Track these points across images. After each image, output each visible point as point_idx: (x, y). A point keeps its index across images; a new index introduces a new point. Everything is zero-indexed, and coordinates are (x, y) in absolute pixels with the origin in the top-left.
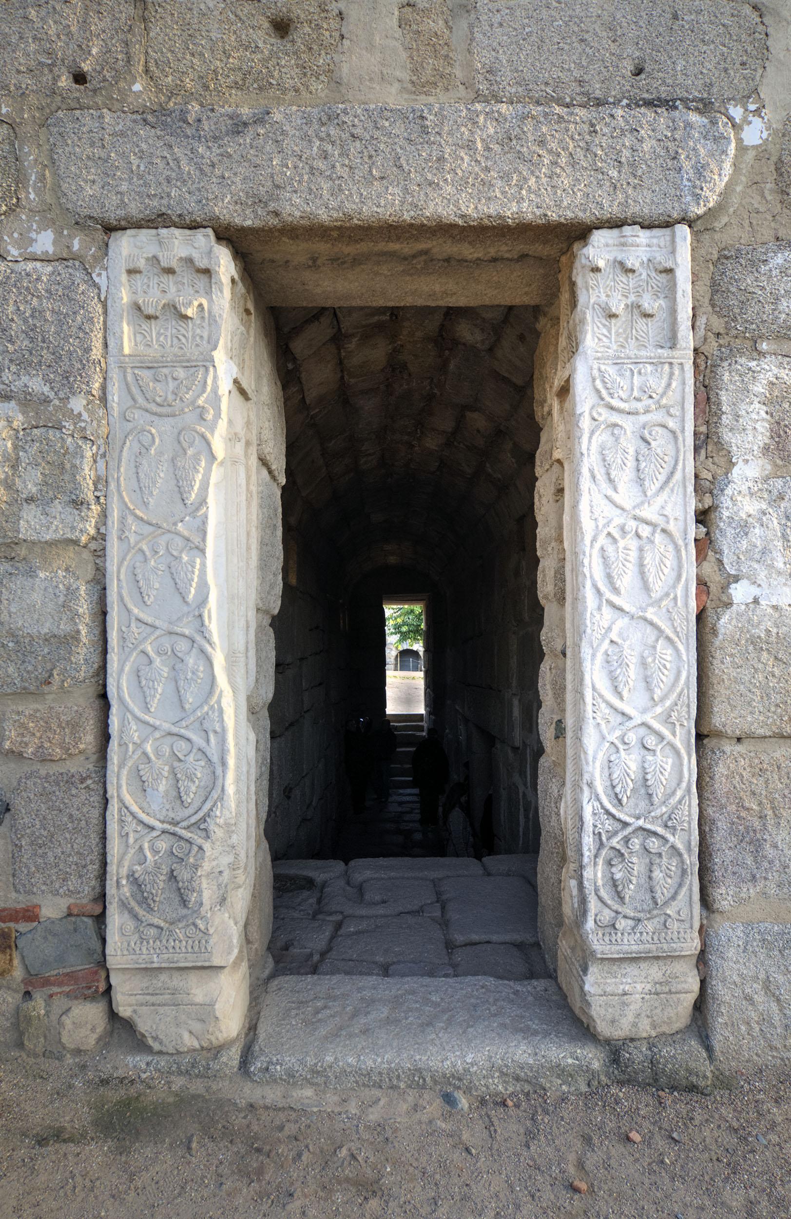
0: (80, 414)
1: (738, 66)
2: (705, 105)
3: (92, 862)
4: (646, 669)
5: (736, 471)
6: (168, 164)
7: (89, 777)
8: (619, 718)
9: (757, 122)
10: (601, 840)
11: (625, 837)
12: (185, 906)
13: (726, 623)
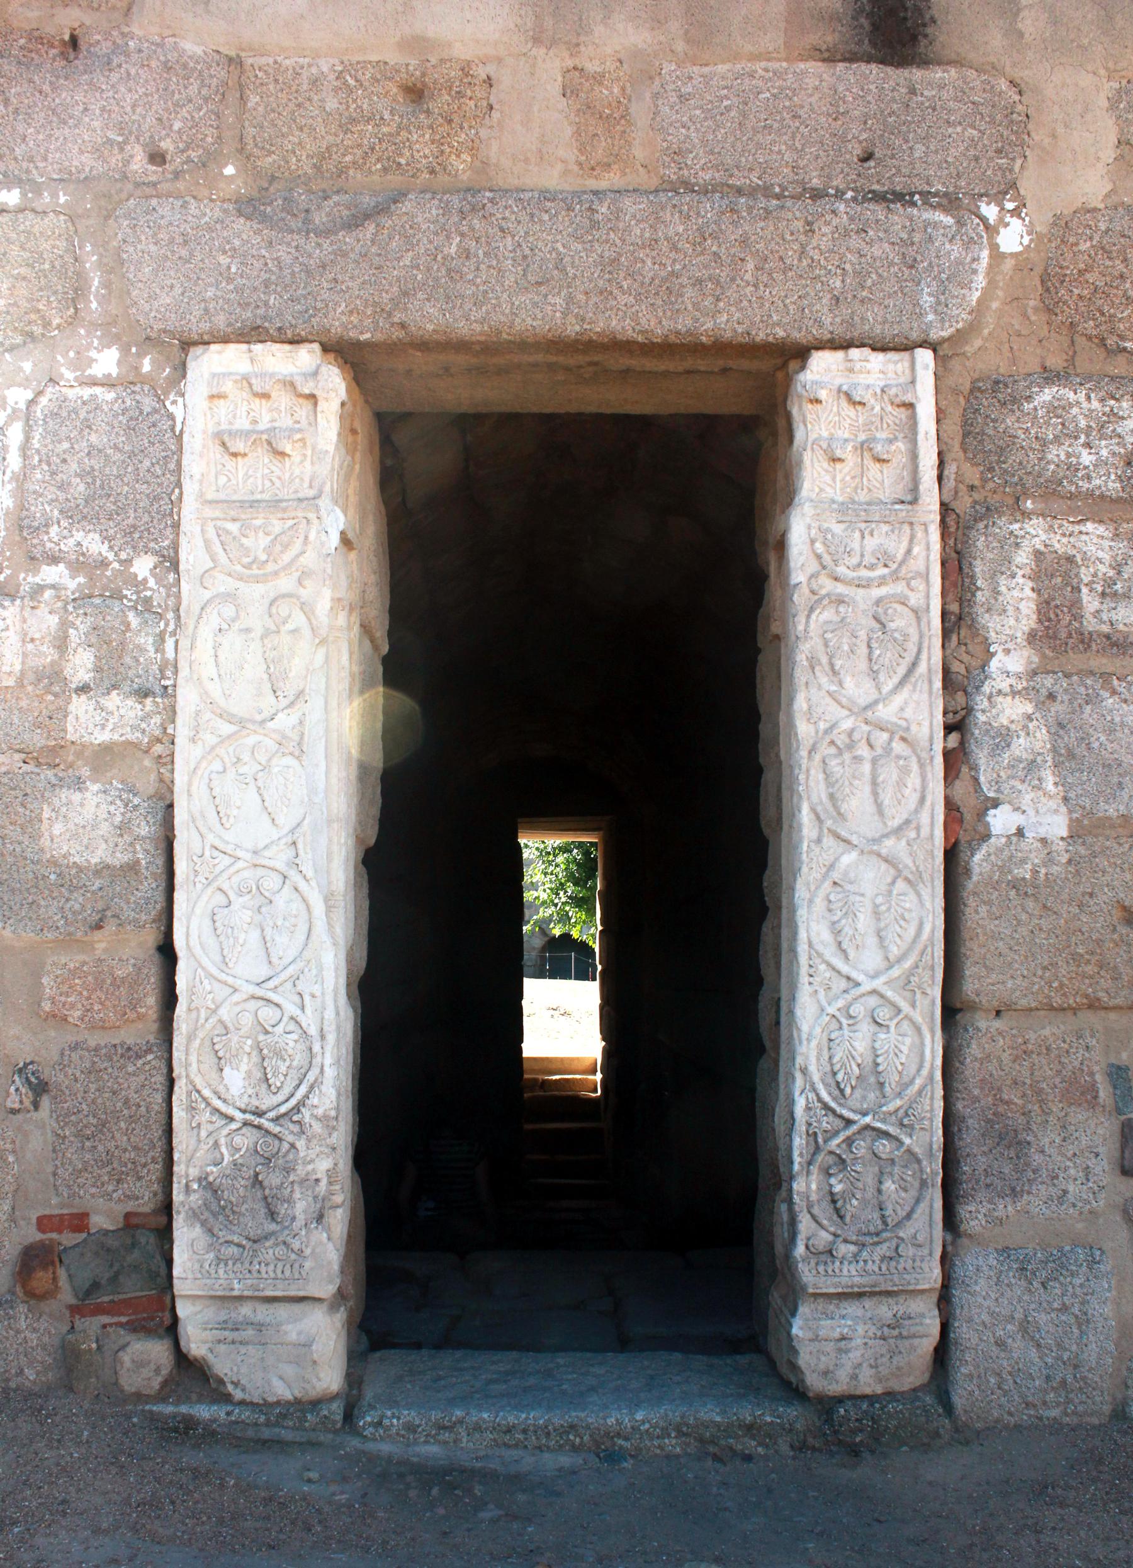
0: (145, 580)
1: (991, 154)
2: (950, 202)
3: (154, 1160)
4: (879, 920)
5: (994, 664)
6: (266, 264)
7: (149, 1051)
8: (843, 984)
9: (1015, 223)
10: (816, 1142)
11: (848, 1138)
12: (273, 1219)
13: (979, 861)
